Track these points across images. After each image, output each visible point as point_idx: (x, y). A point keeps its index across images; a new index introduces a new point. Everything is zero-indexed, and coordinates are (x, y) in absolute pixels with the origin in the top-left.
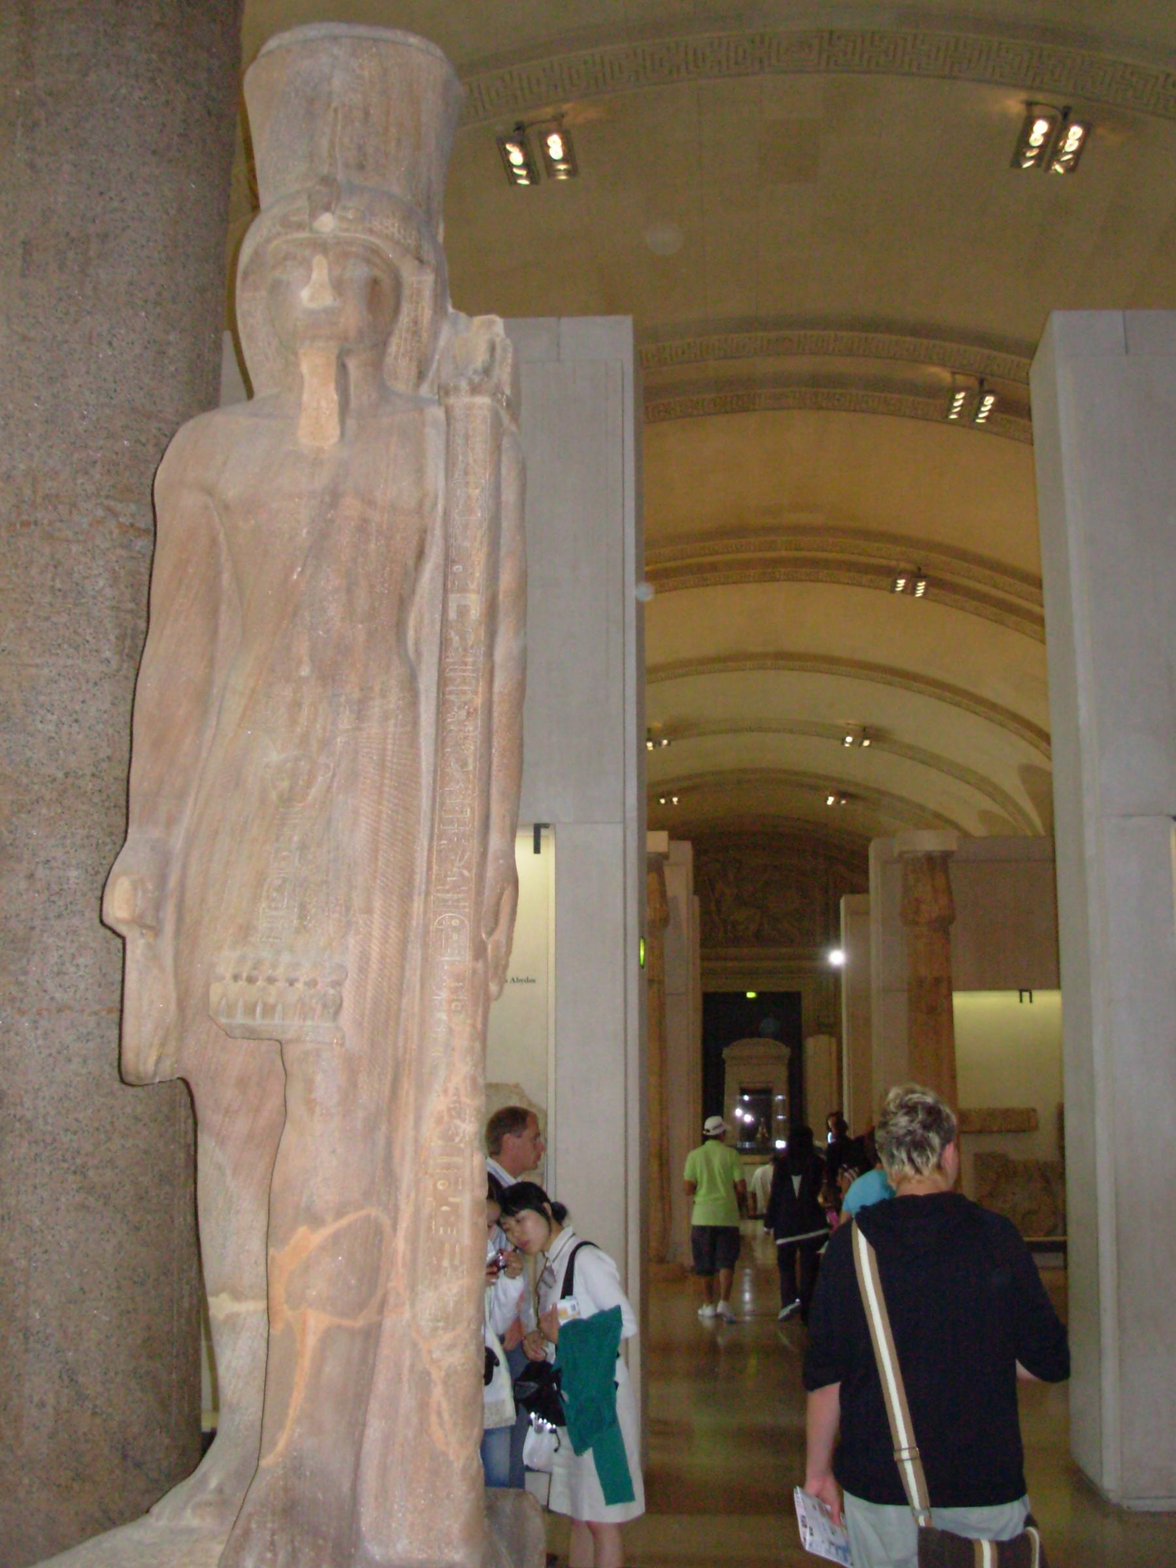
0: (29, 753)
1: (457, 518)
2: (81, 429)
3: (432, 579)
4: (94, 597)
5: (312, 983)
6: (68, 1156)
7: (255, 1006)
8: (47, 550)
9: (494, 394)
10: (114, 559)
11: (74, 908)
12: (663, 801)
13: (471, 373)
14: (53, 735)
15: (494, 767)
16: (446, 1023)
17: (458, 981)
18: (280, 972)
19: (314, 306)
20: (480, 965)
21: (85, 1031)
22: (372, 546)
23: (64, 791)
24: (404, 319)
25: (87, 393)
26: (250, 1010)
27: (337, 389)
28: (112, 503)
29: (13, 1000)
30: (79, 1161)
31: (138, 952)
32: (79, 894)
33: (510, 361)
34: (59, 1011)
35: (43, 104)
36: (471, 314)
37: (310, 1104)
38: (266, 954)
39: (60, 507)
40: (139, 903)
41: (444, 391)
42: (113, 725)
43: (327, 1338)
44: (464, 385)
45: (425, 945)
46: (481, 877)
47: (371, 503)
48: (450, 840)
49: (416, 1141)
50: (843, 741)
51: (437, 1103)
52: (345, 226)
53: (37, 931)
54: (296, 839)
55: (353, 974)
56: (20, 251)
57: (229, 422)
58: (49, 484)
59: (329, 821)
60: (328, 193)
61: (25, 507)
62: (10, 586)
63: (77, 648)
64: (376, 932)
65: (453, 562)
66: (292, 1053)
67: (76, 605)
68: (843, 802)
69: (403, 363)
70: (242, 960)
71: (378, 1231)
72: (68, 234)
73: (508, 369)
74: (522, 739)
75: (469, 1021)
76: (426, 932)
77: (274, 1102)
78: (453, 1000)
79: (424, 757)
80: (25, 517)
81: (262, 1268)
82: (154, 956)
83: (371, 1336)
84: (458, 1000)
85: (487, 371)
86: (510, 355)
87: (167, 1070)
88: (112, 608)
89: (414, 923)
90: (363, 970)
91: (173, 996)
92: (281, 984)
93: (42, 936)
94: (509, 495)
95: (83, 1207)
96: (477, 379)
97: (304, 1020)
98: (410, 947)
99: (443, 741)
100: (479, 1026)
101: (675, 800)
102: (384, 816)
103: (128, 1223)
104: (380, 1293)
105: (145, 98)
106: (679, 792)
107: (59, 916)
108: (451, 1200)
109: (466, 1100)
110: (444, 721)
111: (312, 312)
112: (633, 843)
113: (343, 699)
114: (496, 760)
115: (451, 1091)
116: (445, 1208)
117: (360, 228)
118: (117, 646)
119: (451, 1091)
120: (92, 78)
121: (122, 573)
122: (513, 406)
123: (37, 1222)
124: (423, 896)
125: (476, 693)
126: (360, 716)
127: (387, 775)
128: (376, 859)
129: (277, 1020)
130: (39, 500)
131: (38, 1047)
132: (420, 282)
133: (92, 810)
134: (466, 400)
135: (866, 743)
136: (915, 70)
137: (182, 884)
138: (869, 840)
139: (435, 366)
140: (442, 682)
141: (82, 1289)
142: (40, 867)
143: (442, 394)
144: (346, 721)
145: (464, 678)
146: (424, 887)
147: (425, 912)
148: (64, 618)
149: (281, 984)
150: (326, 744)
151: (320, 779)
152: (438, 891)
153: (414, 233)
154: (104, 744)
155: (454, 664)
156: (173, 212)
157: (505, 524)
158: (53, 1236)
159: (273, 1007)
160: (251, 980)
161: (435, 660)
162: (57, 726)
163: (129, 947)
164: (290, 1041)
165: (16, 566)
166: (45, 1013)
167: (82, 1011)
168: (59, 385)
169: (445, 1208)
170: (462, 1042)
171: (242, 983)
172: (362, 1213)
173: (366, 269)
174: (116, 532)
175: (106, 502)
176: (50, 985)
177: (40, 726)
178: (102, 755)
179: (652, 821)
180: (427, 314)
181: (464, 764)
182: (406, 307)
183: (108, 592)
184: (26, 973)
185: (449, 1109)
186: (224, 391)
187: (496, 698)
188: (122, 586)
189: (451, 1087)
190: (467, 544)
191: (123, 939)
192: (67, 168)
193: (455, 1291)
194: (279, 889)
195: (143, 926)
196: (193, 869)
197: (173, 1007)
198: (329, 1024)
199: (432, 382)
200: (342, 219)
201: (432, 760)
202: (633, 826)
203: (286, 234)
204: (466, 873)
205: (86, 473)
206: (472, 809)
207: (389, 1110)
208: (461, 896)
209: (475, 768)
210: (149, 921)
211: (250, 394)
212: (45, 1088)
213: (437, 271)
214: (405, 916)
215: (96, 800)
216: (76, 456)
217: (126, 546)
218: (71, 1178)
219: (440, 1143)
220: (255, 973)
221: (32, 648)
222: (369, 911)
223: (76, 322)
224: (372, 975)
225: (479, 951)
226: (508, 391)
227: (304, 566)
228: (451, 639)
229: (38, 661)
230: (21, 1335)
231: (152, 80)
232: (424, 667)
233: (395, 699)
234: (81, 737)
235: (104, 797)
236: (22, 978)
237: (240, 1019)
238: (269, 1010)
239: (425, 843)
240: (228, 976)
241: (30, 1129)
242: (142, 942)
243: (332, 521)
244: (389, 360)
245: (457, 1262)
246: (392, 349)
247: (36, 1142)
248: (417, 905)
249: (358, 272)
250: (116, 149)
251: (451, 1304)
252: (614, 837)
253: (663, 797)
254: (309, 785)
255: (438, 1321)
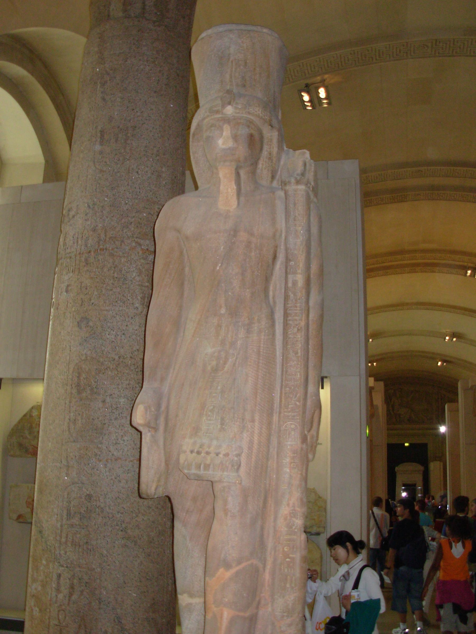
0: (103, 348)
1: (291, 240)
2: (125, 209)
3: (280, 268)
4: (131, 281)
5: (227, 455)
6: (119, 523)
7: (200, 464)
8: (111, 261)
9: (307, 184)
10: (140, 264)
11: (123, 415)
12: (370, 364)
13: (295, 175)
14: (113, 340)
15: (310, 354)
16: (288, 473)
17: (294, 453)
18: (212, 449)
19: (224, 147)
20: (304, 446)
21: (127, 469)
22: (253, 254)
23: (119, 364)
24: (265, 153)
25: (128, 193)
26: (198, 467)
27: (235, 183)
28: (139, 240)
29: (96, 455)
30: (124, 526)
31: (148, 439)
32: (125, 409)
33: (313, 170)
34: (116, 460)
35: (108, 74)
36: (295, 150)
37: (226, 511)
38: (206, 441)
39: (116, 242)
40: (148, 416)
41: (284, 183)
42: (139, 336)
43: (232, 621)
44: (293, 180)
45: (279, 437)
46: (305, 405)
47: (252, 234)
48: (290, 388)
49: (275, 527)
50: (445, 339)
51: (284, 510)
52: (238, 111)
53: (107, 425)
54: (219, 388)
55: (246, 450)
56: (99, 135)
57: (188, 199)
58: (112, 232)
59: (235, 379)
60: (230, 97)
61: (101, 242)
62: (95, 277)
63: (124, 303)
64: (256, 431)
65: (290, 260)
66: (218, 487)
67: (123, 284)
68: (445, 364)
69: (265, 172)
70: (195, 443)
71: (257, 570)
72: (119, 127)
73: (312, 174)
74: (322, 340)
75: (299, 472)
76: (280, 431)
77: (208, 508)
78: (292, 463)
79: (278, 350)
80: (101, 247)
81: (203, 583)
82: (154, 441)
83: (253, 619)
84: (294, 462)
85: (303, 174)
86: (313, 168)
87: (161, 492)
88: (139, 285)
89: (274, 426)
90: (250, 448)
91: (163, 460)
92: (212, 455)
93: (109, 427)
94: (314, 230)
95: (125, 546)
96: (298, 178)
97: (223, 472)
98: (272, 437)
99: (287, 343)
100: (304, 474)
101: (375, 364)
102: (260, 377)
103: (145, 553)
104: (257, 599)
105: (151, 70)
106: (376, 361)
107: (116, 419)
108: (291, 556)
109: (298, 509)
110: (287, 333)
111: (224, 150)
112: (363, 384)
113: (240, 324)
114: (310, 351)
115: (291, 505)
116: (288, 560)
117: (244, 112)
118: (141, 301)
119: (291, 505)
120: (129, 62)
121: (143, 270)
122: (315, 190)
123: (105, 552)
124: (278, 414)
125: (301, 320)
126: (249, 331)
127: (261, 358)
128: (256, 397)
129: (211, 472)
130: (107, 239)
131: (107, 476)
132: (271, 136)
133: (130, 372)
134: (294, 187)
135: (454, 339)
136: (472, 54)
137: (168, 407)
138: (458, 381)
139: (279, 172)
140: (286, 315)
141: (124, 582)
142: (108, 398)
143: (283, 185)
144: (242, 333)
145: (296, 313)
146: (278, 410)
147: (279, 421)
148: (119, 290)
149: (212, 455)
150: (233, 344)
151: (230, 360)
152: (285, 412)
153: (269, 114)
154: (136, 344)
155: (291, 307)
156: (163, 117)
157: (313, 243)
158: (112, 559)
159: (209, 465)
160: (199, 453)
161: (282, 305)
162: (115, 336)
163: (143, 436)
164: (216, 482)
165: (98, 268)
166: (109, 461)
167: (126, 460)
168: (116, 190)
169: (288, 560)
170: (296, 482)
171: (194, 454)
172: (249, 562)
173: (248, 130)
174: (141, 252)
175: (136, 240)
176: (112, 448)
177: (108, 337)
178: (135, 349)
179: (371, 373)
180: (275, 150)
181: (297, 353)
182: (266, 147)
183: (138, 278)
184: (101, 443)
185: (290, 513)
186: (187, 186)
187: (310, 322)
188: (143, 276)
189: (291, 503)
190: (296, 252)
191: (141, 433)
192: (119, 100)
193: (292, 598)
194: (212, 411)
195: (149, 427)
196: (172, 402)
197: (163, 464)
198: (235, 474)
199: (278, 180)
200: (236, 108)
201: (281, 351)
202: (364, 377)
203: (211, 116)
204: (298, 403)
205: (128, 227)
206: (301, 375)
207: (262, 514)
208: (295, 414)
209: (301, 355)
210: (153, 425)
211: (196, 188)
212: (109, 494)
213: (279, 131)
214: (270, 424)
215: (132, 368)
216: (123, 220)
217: (144, 259)
218: (120, 533)
219: (286, 529)
220: (200, 449)
221: (105, 303)
222: (253, 421)
223: (123, 163)
224: (255, 451)
225: (304, 439)
226: (312, 184)
227: (222, 264)
228: (289, 296)
229: (107, 308)
230: (97, 601)
231: (154, 62)
232: (277, 308)
233: (264, 323)
234: (125, 341)
235: (136, 367)
236: (100, 446)
237: (193, 471)
238: (207, 467)
239: (279, 389)
240: (188, 451)
241: (102, 512)
242: (149, 434)
243: (234, 243)
244: (258, 171)
245: (293, 585)
246: (260, 166)
247: (105, 517)
248: (275, 418)
249: (243, 131)
250: (139, 91)
251: (290, 604)
252: (356, 382)
253: (370, 363)
254: (225, 363)
255: (284, 613)
